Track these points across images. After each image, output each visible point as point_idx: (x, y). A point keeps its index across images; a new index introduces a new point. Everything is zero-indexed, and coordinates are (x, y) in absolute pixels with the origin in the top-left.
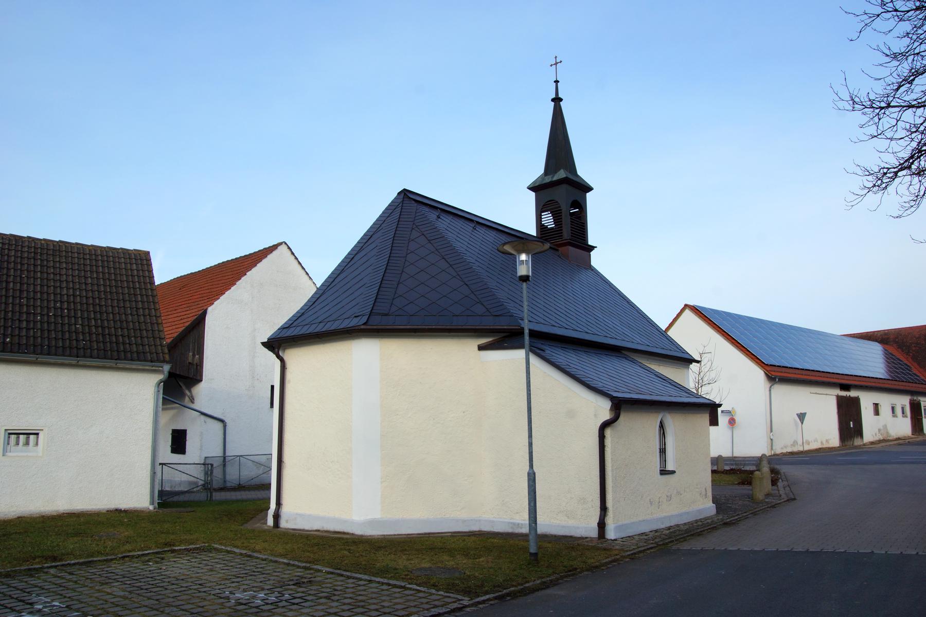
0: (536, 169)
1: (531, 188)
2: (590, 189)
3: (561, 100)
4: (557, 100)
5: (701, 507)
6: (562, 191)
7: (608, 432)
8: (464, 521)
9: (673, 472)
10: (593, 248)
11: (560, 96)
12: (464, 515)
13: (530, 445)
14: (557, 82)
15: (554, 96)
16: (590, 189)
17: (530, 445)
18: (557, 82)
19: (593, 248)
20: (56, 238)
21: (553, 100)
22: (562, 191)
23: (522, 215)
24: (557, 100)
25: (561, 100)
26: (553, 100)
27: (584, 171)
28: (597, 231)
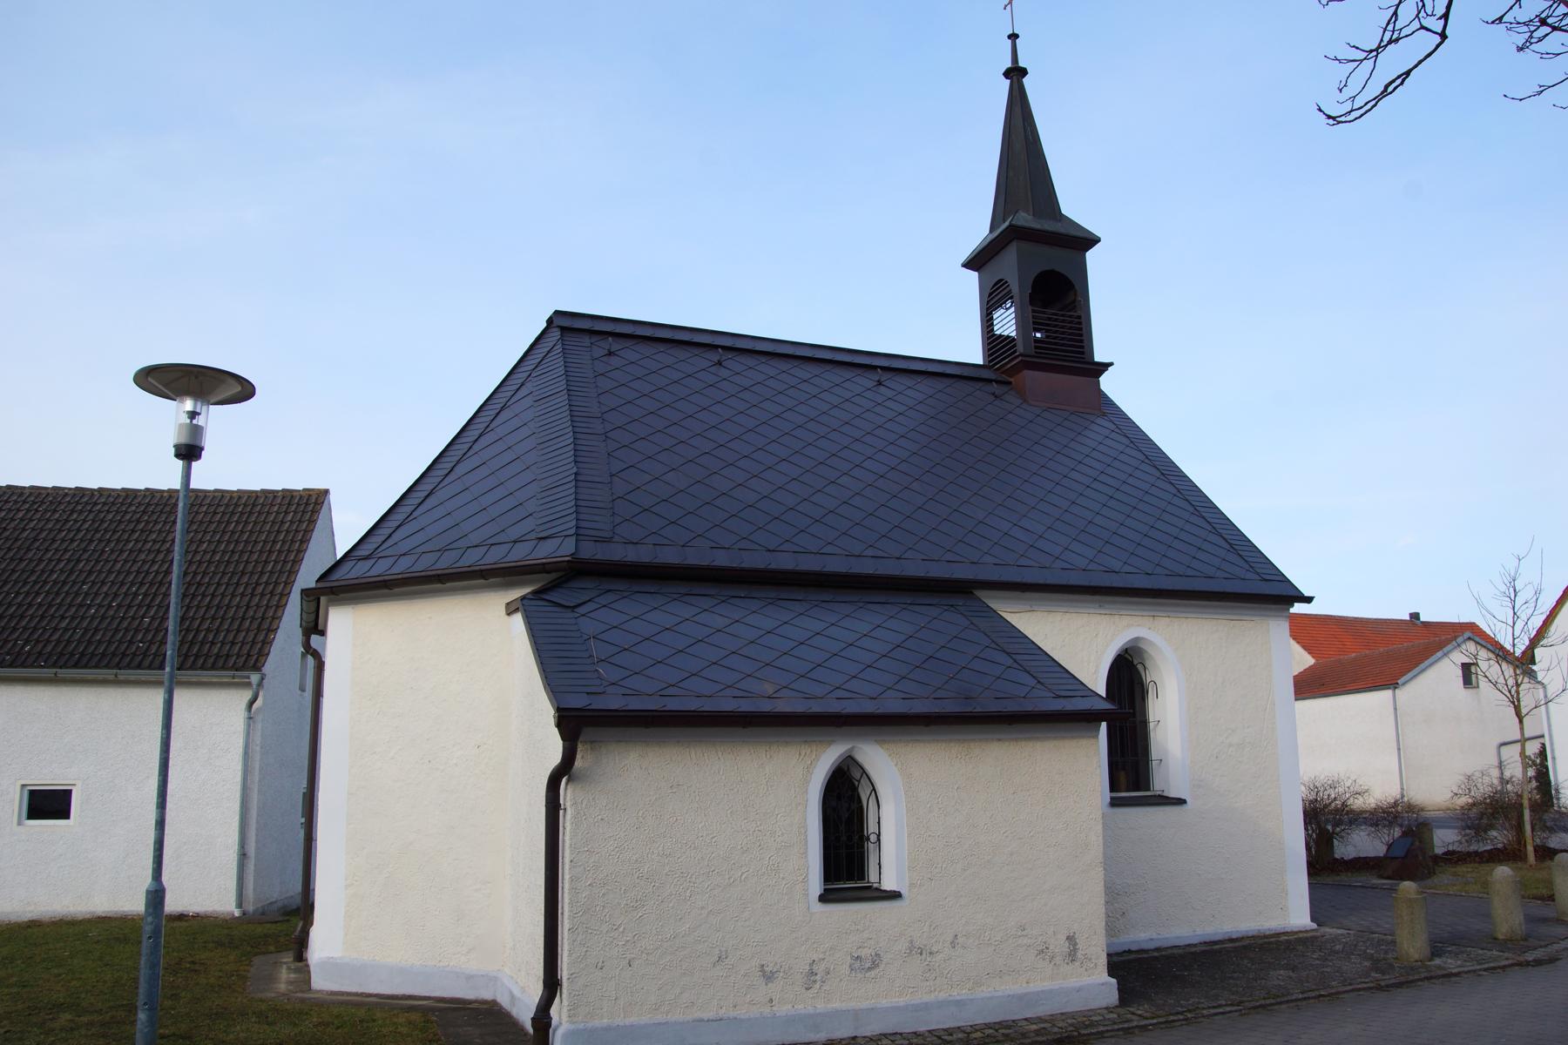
0: (977, 229)
1: (968, 265)
2: (1092, 241)
3: (1024, 72)
4: (1016, 73)
5: (1038, 985)
6: (1037, 259)
7: (567, 793)
8: (469, 977)
9: (895, 896)
10: (1105, 366)
11: (1021, 64)
12: (473, 965)
13: (161, 824)
14: (1013, 37)
15: (1009, 65)
16: (1092, 241)
17: (161, 824)
18: (1013, 37)
19: (1105, 366)
20: (256, 486)
21: (1007, 74)
22: (1037, 259)
23: (945, 322)
24: (1016, 73)
25: (1024, 72)
26: (1007, 74)
27: (1075, 204)
28: (1108, 335)
